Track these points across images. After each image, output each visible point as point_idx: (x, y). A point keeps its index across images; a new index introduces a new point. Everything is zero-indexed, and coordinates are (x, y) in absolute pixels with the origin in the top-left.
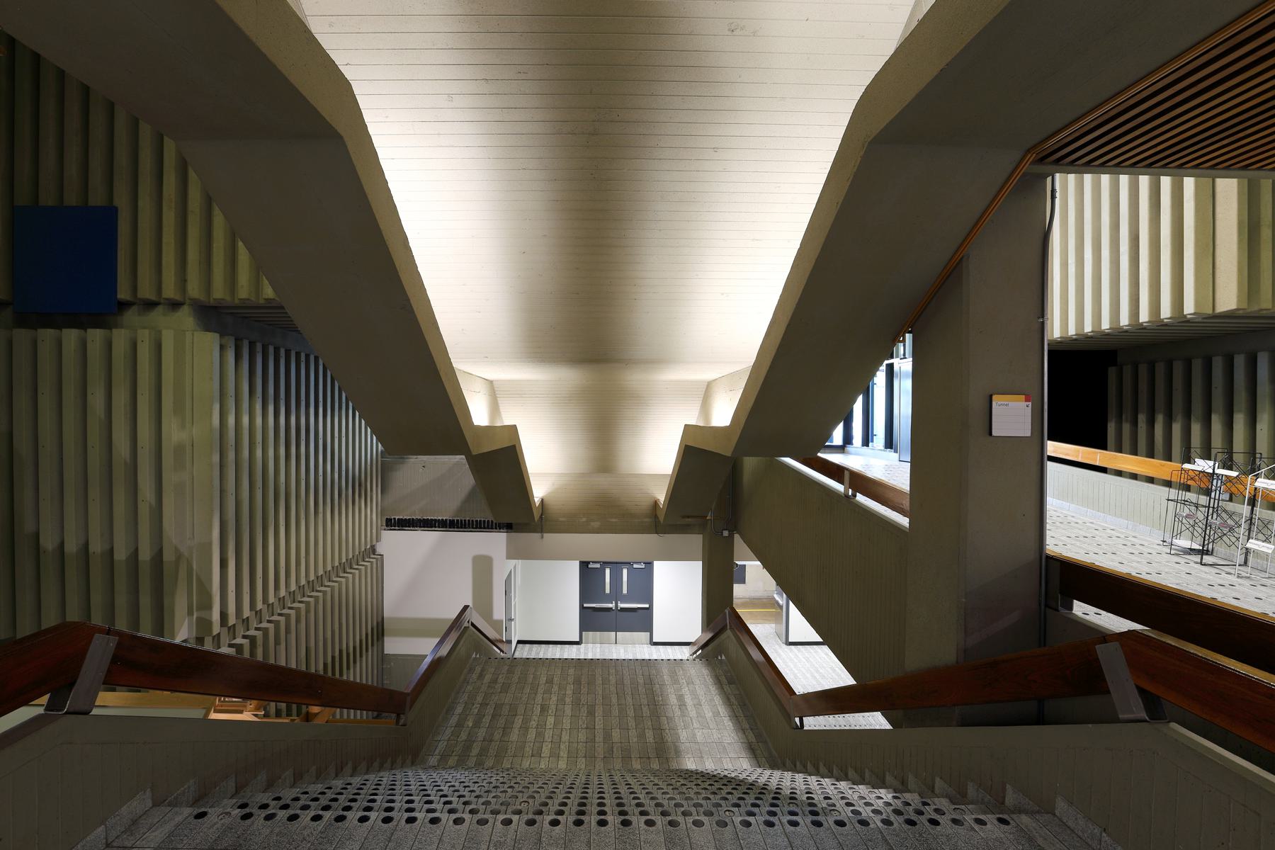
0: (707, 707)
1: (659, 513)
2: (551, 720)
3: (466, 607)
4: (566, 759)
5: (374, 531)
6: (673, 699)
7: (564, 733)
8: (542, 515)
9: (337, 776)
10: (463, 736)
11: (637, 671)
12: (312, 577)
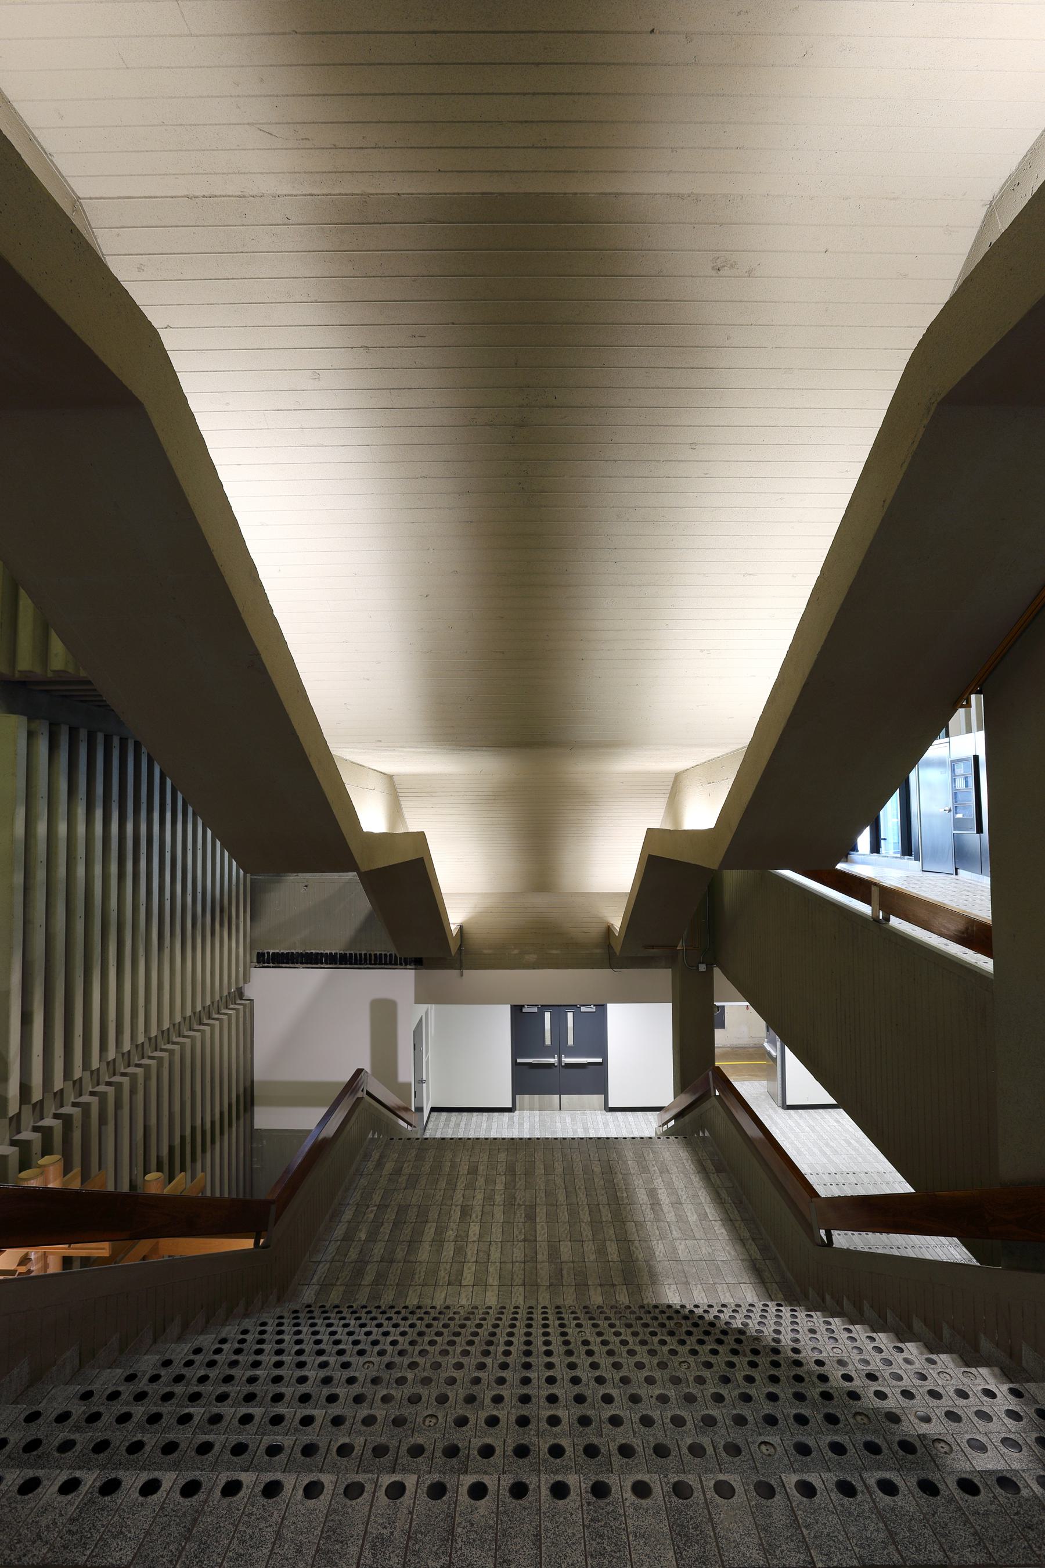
0: (690, 1206)
1: (613, 944)
2: (475, 1229)
3: (359, 1071)
4: (496, 1288)
5: (241, 969)
6: (642, 1196)
7: (493, 1248)
8: (461, 946)
9: (155, 1342)
10: (353, 1254)
11: (592, 1155)
12: (154, 1033)
